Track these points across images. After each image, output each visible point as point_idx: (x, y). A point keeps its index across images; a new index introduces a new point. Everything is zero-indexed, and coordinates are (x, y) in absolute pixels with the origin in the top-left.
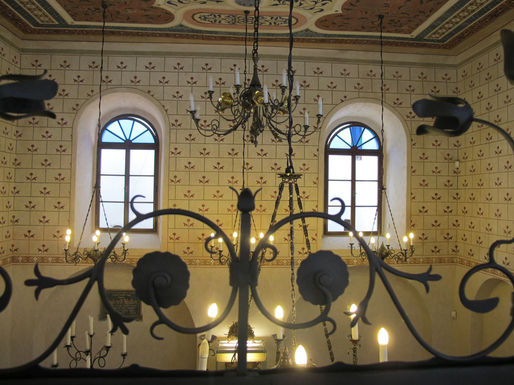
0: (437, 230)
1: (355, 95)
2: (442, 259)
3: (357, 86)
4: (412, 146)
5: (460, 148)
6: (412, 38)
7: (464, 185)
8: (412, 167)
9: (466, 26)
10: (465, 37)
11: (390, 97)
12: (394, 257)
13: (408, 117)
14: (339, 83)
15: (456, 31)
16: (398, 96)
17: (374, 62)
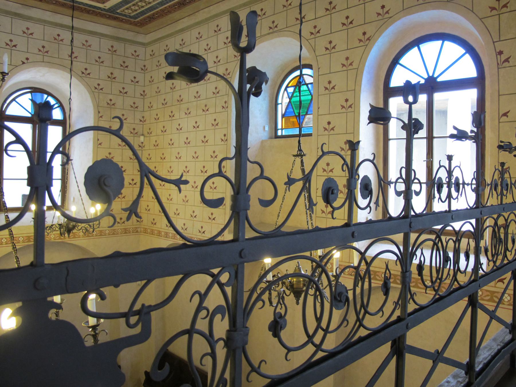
0: (122, 202)
1: (39, 58)
2: (127, 229)
3: (42, 49)
4: (98, 119)
5: (145, 123)
6: (104, 9)
7: (148, 159)
8: (98, 140)
9: (157, 8)
10: (156, 19)
11: (78, 66)
12: (81, 229)
13: (96, 88)
14: (21, 42)
15: (148, 10)
16: (87, 66)
17: (62, 26)
